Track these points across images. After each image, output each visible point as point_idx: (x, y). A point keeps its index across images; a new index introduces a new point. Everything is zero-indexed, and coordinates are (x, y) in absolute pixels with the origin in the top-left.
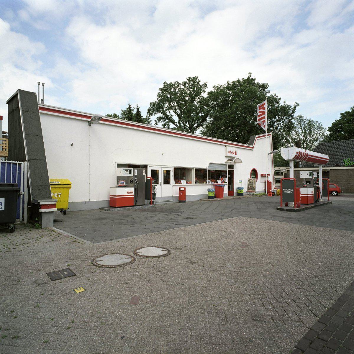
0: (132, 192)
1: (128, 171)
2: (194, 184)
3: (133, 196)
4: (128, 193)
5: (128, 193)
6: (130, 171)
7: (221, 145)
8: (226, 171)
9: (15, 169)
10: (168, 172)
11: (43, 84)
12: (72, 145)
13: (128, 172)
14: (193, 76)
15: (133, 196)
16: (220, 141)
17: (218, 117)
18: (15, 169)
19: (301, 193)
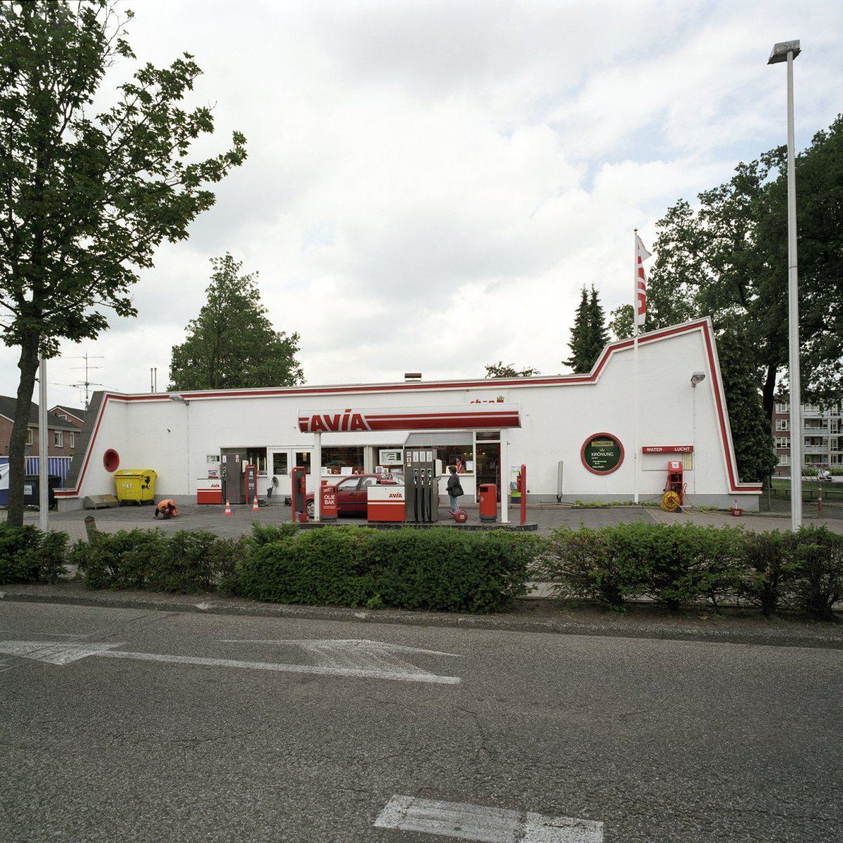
0: (400, 496)
1: (395, 455)
2: (329, 475)
3: (404, 503)
4: (391, 496)
5: (391, 496)
6: (399, 454)
7: (387, 393)
8: (472, 446)
9: (35, 462)
10: (835, 457)
11: (156, 369)
12: (169, 431)
13: (396, 458)
14: (202, 307)
15: (404, 503)
16: (506, 381)
17: (767, 301)
18: (35, 462)
19: (369, 499)
